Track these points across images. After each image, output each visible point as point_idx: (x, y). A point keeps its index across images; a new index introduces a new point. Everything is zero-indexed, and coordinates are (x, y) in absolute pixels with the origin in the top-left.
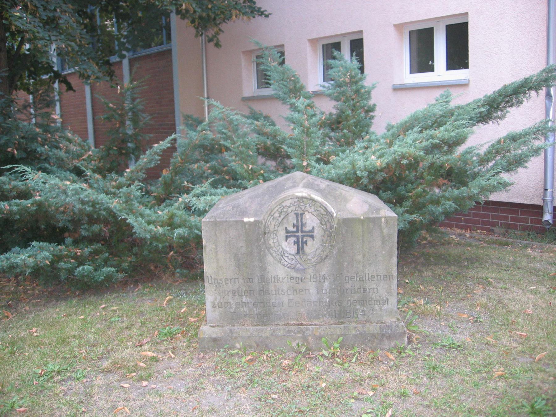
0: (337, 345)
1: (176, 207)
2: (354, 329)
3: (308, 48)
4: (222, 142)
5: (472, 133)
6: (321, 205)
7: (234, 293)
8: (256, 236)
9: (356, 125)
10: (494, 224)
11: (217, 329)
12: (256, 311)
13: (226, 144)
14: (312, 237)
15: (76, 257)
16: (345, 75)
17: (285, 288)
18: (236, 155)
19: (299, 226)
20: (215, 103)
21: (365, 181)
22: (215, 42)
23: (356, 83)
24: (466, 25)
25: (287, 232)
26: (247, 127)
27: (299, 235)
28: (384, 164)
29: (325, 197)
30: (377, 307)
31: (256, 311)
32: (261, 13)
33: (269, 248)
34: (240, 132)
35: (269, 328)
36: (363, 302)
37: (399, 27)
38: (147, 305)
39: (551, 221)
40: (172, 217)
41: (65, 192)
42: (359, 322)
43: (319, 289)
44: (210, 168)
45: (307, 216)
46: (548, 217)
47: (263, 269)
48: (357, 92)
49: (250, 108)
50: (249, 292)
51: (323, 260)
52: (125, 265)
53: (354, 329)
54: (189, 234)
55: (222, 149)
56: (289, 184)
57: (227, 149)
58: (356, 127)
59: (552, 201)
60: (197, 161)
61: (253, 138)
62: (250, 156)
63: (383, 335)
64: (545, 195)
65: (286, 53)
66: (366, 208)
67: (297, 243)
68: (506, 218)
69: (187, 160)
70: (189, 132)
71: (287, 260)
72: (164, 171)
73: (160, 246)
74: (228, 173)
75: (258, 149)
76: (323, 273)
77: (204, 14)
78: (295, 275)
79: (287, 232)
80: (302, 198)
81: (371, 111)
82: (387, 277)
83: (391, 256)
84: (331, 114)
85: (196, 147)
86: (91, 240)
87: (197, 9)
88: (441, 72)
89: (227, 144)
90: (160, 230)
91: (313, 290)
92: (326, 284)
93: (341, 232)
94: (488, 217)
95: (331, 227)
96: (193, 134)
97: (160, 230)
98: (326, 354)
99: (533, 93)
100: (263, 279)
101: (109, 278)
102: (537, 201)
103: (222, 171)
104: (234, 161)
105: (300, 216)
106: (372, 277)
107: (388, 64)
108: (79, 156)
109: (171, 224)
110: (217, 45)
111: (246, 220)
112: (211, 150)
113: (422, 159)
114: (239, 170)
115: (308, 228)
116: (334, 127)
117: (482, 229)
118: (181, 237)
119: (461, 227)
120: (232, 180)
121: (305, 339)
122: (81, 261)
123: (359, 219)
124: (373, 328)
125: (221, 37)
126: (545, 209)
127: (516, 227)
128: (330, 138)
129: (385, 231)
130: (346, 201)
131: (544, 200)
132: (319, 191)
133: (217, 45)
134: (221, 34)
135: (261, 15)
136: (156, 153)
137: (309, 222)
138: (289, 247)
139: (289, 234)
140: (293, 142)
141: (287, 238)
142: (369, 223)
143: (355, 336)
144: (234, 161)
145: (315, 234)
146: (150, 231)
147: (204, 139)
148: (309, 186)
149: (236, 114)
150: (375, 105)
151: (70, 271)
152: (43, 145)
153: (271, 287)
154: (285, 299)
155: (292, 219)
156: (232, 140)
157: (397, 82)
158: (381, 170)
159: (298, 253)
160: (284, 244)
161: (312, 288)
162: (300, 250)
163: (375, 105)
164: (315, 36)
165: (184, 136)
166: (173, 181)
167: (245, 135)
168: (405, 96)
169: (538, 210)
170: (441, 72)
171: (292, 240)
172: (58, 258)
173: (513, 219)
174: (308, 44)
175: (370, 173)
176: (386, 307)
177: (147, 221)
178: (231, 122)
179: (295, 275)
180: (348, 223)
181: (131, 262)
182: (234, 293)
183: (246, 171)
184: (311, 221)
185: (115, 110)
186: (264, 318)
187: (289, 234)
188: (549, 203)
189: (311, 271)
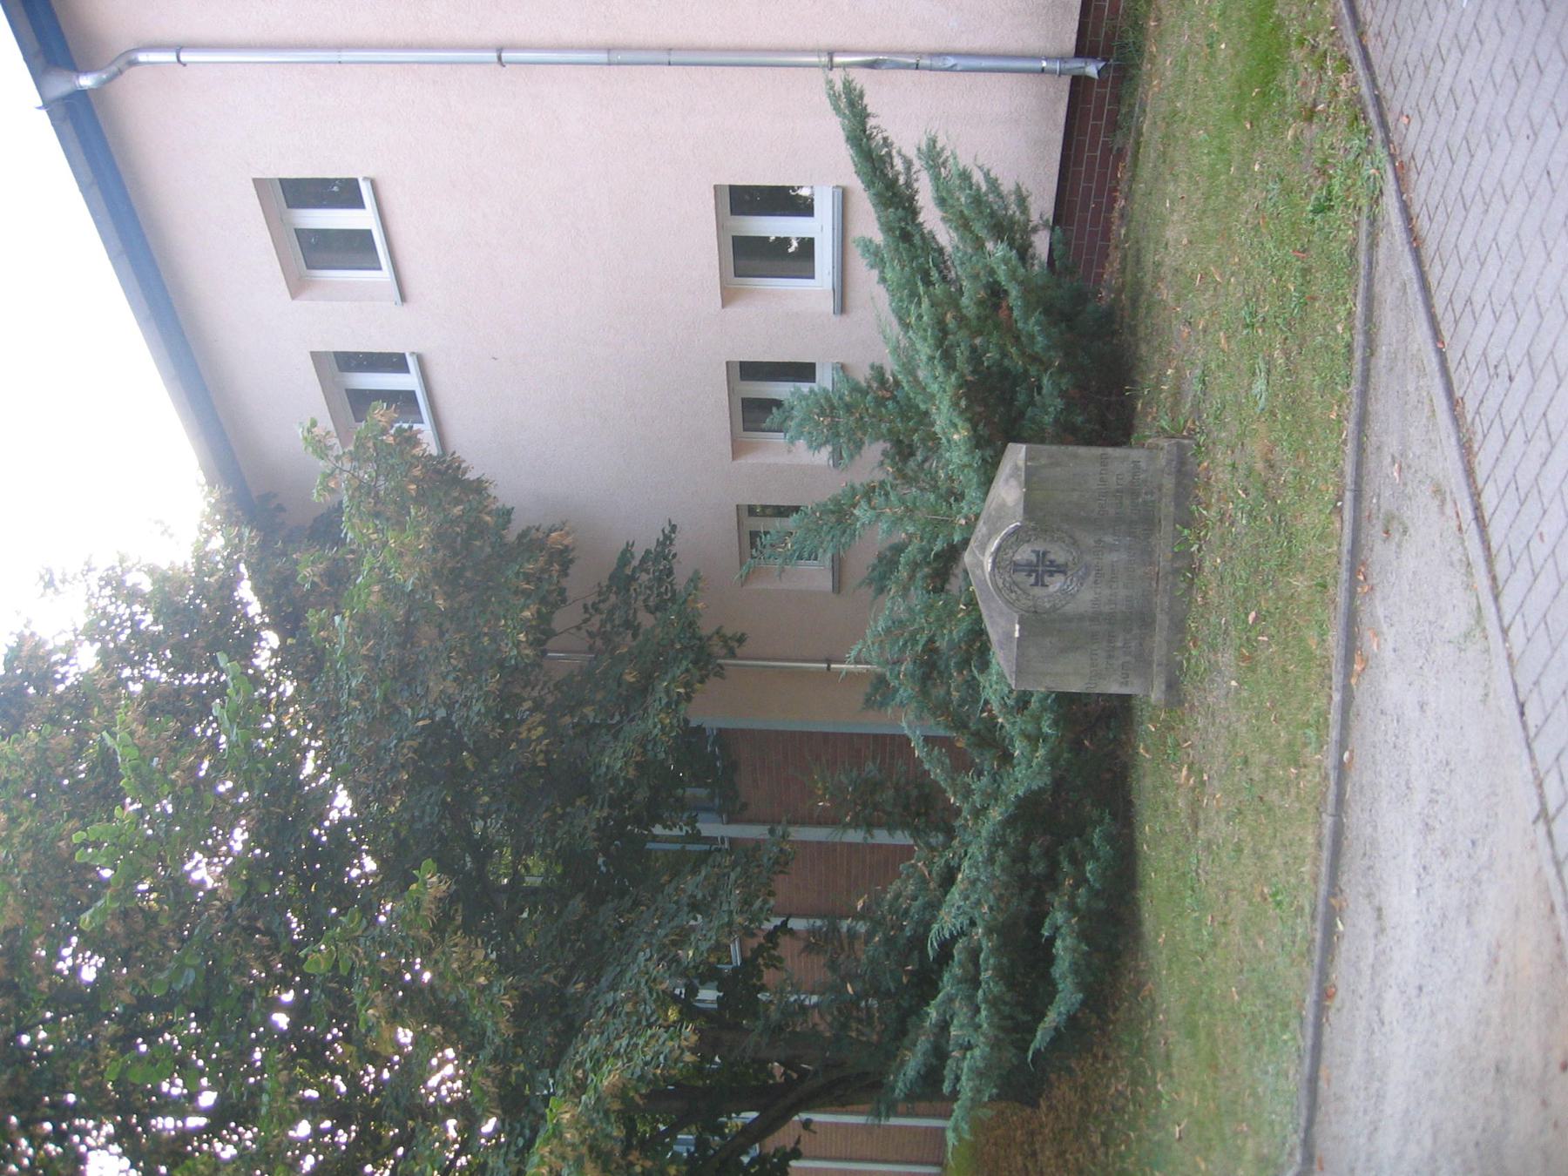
0: (1186, 532)
1: (1012, 727)
2: (1167, 507)
3: (749, 461)
4: (919, 648)
5: (933, 156)
6: (1003, 540)
7: (1110, 657)
8: (1037, 623)
9: (905, 418)
10: (1107, 150)
11: (1156, 683)
12: (1136, 631)
13: (922, 642)
14: (1045, 554)
15: (1076, 886)
16: (817, 424)
17: (1107, 592)
18: (943, 627)
19: (1030, 568)
20: (853, 653)
21: (989, 452)
22: (735, 644)
23: (833, 408)
24: (732, 188)
25: (1036, 584)
26: (892, 606)
27: (1042, 569)
28: (968, 425)
29: (997, 531)
30: (1142, 476)
31: (1136, 631)
32: (667, 540)
33: (1054, 609)
34: (905, 616)
35: (1159, 617)
36: (1134, 494)
37: (728, 296)
38: (1148, 782)
39: (1101, 65)
40: (1028, 737)
41: (973, 882)
42: (1160, 500)
43: (1112, 548)
44: (960, 672)
45: (1017, 557)
46: (1092, 70)
47: (1081, 618)
48: (849, 408)
49: (860, 586)
50: (1111, 638)
51: (1075, 543)
52: (1095, 814)
53: (1167, 507)
54: (1052, 711)
55: (931, 648)
56: (978, 572)
57: (931, 640)
58: (910, 419)
59: (1062, 59)
60: (949, 693)
61: (917, 597)
62: (945, 605)
63: (1179, 471)
64: (1053, 72)
65: (754, 502)
66: (1013, 482)
67: (1051, 574)
68: (1096, 128)
69: (942, 708)
70: (898, 700)
71: (1073, 588)
72: (958, 745)
73: (1065, 755)
74: (970, 644)
75: (935, 590)
76: (1092, 542)
77: (692, 656)
78: (1091, 578)
79: (1036, 584)
80: (994, 562)
81: (883, 375)
82: (1104, 461)
83: (1076, 456)
84: (885, 453)
85: (924, 692)
86: (1054, 865)
87: (683, 668)
88: (819, 227)
89: (922, 639)
90: (1041, 752)
91: (1114, 557)
92: (1109, 539)
93: (1040, 514)
94: (1091, 160)
95: (1034, 529)
96: (903, 694)
97: (1041, 752)
98: (1196, 547)
99: (871, 122)
100: (1095, 618)
101: (1109, 839)
102: (1065, 84)
103: (967, 651)
104: (951, 632)
105: (1017, 567)
106: (1102, 480)
107: (789, 315)
108: (924, 881)
109: (1034, 739)
110: (741, 640)
111: (1017, 634)
112: (930, 667)
113: (962, 376)
114: (965, 626)
115: (1034, 558)
116: (907, 451)
117: (1116, 168)
118: (1055, 723)
119: (1110, 209)
120: (977, 646)
121: (1176, 572)
122: (1081, 880)
123: (1026, 495)
124: (1169, 483)
125: (728, 632)
126: (1076, 73)
127: (1113, 114)
128: (924, 461)
129: (1043, 461)
130: (1003, 505)
131: (1061, 73)
132: (990, 536)
133: (741, 640)
134: (724, 631)
135: (672, 541)
136: (929, 754)
137: (1026, 556)
138: (1056, 584)
139: (1040, 582)
140: (927, 536)
141: (1044, 585)
142: (1031, 479)
143: (1177, 506)
144: (951, 632)
145: (1041, 550)
146: (1041, 767)
147: (913, 676)
148: (983, 548)
149: (876, 621)
150: (872, 367)
151: (1096, 894)
152: (902, 928)
153: (1106, 609)
154: (1122, 593)
155: (1021, 577)
156: (917, 632)
157: (828, 305)
158: (974, 428)
159: (1064, 573)
160: (1051, 589)
161: (1110, 558)
162: (1061, 569)
163: (872, 367)
164: (727, 448)
165: (907, 721)
166: (976, 734)
167: (910, 610)
168: (857, 296)
169: (1079, 84)
170: (819, 227)
171: (1047, 579)
172: (1072, 908)
173: (1098, 117)
174: (741, 461)
175: (978, 446)
176: (1143, 465)
177: (1028, 772)
178: (888, 631)
179: (1091, 578)
180: (1030, 507)
181: (1093, 805)
182: (1110, 657)
183: (969, 614)
184: (1025, 554)
185: (857, 814)
186: (1143, 620)
187: (1040, 582)
188: (1068, 66)
189: (1088, 558)
